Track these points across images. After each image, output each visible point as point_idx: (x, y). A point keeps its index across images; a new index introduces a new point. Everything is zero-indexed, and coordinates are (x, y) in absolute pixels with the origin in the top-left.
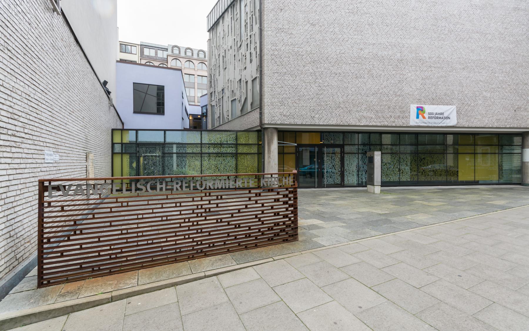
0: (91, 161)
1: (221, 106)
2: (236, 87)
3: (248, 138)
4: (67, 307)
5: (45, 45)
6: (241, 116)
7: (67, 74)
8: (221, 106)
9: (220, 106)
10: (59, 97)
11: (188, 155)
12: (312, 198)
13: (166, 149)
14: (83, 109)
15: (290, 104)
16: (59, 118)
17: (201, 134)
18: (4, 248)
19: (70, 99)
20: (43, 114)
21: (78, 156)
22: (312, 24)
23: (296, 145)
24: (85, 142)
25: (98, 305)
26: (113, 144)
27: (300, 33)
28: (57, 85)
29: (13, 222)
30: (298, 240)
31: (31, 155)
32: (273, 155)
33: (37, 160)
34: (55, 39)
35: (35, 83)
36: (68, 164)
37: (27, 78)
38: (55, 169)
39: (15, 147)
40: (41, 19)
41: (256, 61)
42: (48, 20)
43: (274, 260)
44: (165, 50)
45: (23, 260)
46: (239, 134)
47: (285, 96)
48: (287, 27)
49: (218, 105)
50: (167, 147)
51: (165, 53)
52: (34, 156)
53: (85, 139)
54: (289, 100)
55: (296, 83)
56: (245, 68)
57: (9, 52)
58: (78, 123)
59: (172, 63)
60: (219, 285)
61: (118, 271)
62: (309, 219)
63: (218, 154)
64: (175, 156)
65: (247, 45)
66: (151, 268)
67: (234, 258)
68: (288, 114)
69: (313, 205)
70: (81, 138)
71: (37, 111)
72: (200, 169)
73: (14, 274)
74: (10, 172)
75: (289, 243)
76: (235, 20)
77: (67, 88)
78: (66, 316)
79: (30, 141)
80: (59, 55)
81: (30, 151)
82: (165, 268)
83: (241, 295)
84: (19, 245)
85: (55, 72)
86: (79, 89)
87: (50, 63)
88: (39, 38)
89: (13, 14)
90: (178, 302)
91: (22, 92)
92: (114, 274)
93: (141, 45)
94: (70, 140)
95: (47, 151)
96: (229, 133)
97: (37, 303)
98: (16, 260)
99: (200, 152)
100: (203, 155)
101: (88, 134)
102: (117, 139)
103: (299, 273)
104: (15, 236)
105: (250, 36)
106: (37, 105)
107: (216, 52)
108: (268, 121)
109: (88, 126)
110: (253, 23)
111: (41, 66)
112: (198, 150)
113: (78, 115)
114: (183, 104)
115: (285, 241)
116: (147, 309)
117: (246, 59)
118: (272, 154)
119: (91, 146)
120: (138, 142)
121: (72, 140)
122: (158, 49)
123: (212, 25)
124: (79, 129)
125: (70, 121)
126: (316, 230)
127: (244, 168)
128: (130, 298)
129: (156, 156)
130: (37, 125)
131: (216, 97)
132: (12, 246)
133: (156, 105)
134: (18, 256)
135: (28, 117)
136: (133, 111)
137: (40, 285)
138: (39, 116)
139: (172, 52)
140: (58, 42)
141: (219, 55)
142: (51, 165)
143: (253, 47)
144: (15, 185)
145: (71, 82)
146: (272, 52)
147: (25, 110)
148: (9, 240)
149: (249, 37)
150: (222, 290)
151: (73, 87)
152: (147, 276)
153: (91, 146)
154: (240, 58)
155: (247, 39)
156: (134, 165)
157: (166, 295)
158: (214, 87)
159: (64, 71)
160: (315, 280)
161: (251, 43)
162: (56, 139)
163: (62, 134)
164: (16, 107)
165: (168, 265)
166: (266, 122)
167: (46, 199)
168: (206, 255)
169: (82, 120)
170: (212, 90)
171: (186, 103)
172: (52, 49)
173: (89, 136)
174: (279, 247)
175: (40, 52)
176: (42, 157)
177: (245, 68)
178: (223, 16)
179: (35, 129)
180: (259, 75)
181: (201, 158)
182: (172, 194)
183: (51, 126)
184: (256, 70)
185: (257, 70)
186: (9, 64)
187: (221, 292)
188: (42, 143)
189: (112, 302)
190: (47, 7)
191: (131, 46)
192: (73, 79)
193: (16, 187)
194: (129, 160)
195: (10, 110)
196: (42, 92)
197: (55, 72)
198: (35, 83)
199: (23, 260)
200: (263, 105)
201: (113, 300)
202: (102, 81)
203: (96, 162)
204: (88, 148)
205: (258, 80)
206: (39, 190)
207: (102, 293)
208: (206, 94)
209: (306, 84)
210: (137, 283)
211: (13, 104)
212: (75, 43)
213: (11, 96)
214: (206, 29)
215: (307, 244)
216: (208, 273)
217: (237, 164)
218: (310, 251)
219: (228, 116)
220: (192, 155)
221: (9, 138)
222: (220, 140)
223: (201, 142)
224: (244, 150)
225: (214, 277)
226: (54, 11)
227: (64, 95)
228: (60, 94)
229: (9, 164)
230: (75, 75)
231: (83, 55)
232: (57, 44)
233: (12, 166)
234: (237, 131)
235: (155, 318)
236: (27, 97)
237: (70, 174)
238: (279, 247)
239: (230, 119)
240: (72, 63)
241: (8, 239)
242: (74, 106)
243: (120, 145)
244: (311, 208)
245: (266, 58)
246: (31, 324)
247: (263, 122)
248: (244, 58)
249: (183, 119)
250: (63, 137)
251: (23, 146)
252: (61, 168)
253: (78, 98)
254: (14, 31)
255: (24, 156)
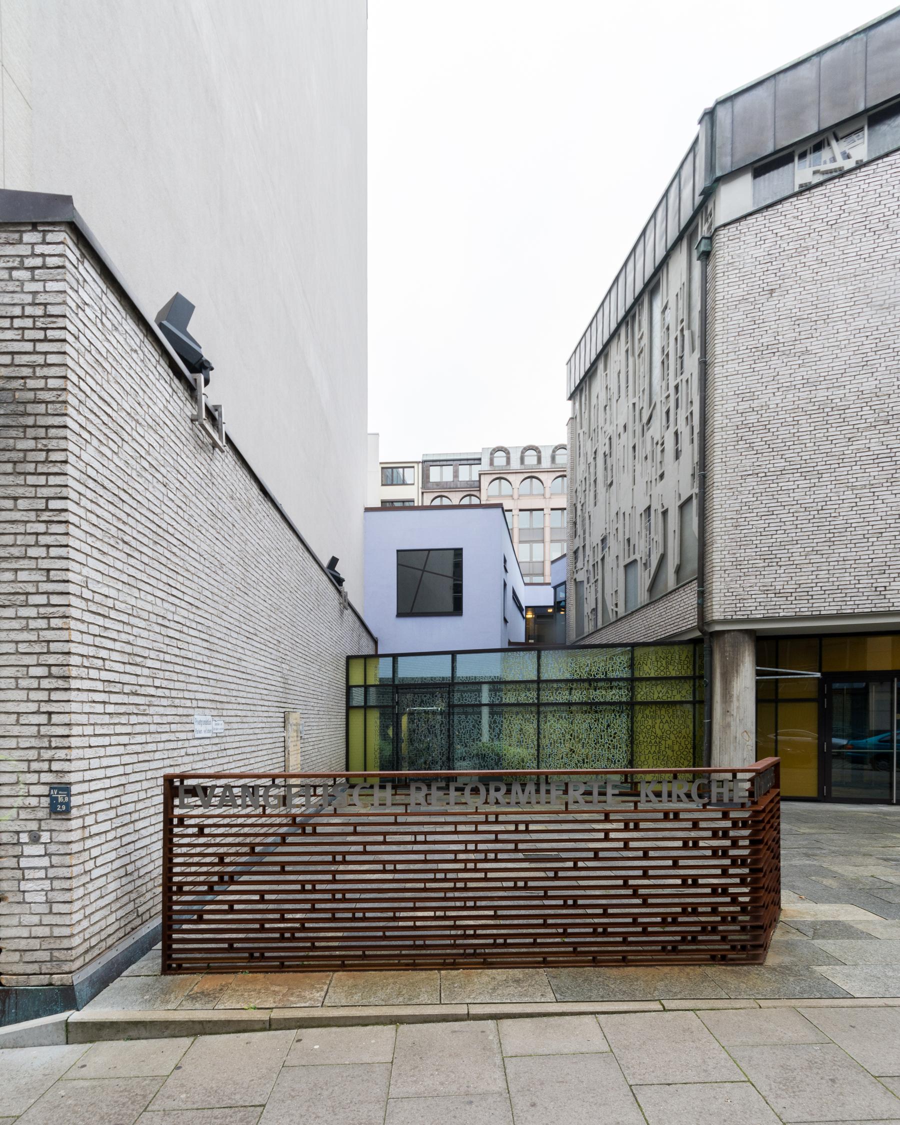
0: (295, 728)
1: (600, 582)
2: (638, 529)
3: (664, 662)
4: (193, 1022)
5: (196, 517)
6: (647, 605)
7: (241, 562)
8: (600, 582)
9: (596, 581)
10: (225, 610)
11: (505, 709)
12: (867, 836)
13: (457, 696)
14: (278, 624)
15: (797, 559)
16: (225, 651)
17: (539, 658)
18: (115, 893)
19: (248, 610)
20: (192, 648)
21: (265, 720)
22: (882, 307)
23: (818, 675)
24: (281, 690)
25: (245, 1031)
26: (349, 688)
27: (838, 343)
28: (221, 587)
29: (131, 847)
30: (761, 964)
31: (168, 726)
32: (738, 708)
33: (177, 735)
34: (218, 500)
35: (175, 592)
36: (243, 738)
37: (161, 585)
38: (215, 748)
39: (137, 714)
40: (188, 469)
41: (690, 452)
42: (202, 468)
43: (665, 1010)
44: (476, 462)
45: (151, 917)
46: (639, 652)
47: (780, 537)
48: (791, 335)
49: (592, 581)
50: (458, 691)
51: (476, 469)
52: (174, 727)
53: (282, 685)
54: (795, 549)
55: (821, 493)
56: (662, 476)
57: (126, 546)
58: (266, 654)
59: (489, 492)
60: (495, 1046)
61: (298, 966)
62: (828, 901)
63: (592, 706)
64: (485, 711)
65: (668, 412)
66: (358, 973)
67: (554, 982)
68: (790, 588)
69: (860, 860)
70: (274, 683)
71: (180, 644)
72: (536, 743)
73: (133, 942)
74: (126, 759)
75: (729, 968)
76: (637, 353)
77: (243, 588)
78: (192, 1039)
79: (166, 700)
80: (225, 528)
81: (165, 720)
82: (387, 979)
83: (542, 1084)
84: (144, 889)
85: (216, 563)
86: (269, 586)
87: (207, 548)
88: (183, 506)
89: (134, 475)
90: (392, 1062)
91: (149, 612)
92: (288, 972)
93: (424, 462)
94: (248, 689)
95: (198, 716)
96: (612, 651)
97: (152, 1002)
98: (138, 916)
99: (536, 701)
100: (542, 709)
101: (289, 673)
102: (357, 678)
103: (731, 1062)
104: (136, 875)
105: (677, 387)
106: (180, 632)
107: (588, 447)
108: (724, 612)
109: (288, 658)
110: (683, 351)
111: (187, 558)
112: (529, 696)
113: (266, 638)
114: (505, 585)
115: (718, 959)
116: (327, 1062)
117: (663, 451)
118: (735, 704)
119: (296, 697)
120: (396, 683)
121: (253, 690)
122: (459, 462)
123: (578, 382)
124: (268, 666)
125: (247, 652)
126: (839, 942)
127: (653, 741)
128: (304, 1030)
129: (434, 713)
130: (178, 669)
131: (586, 559)
132: (131, 892)
133: (452, 591)
134: (141, 910)
135: (161, 656)
136: (395, 613)
137: (167, 969)
138: (183, 653)
139: (492, 463)
140: (223, 504)
141: (595, 453)
142: (207, 742)
143: (684, 417)
144: (137, 782)
145: (250, 576)
146: (737, 420)
147: (155, 644)
148: (124, 881)
149: (672, 391)
150: (498, 1061)
151: (255, 585)
152: (346, 988)
153: (296, 697)
154: (648, 452)
155: (668, 397)
156: (390, 732)
157: (373, 1041)
158: (582, 536)
159: (236, 558)
160: (778, 1096)
161: (677, 407)
162: (218, 691)
163: (231, 679)
164: (139, 642)
165: (395, 972)
166: (717, 615)
167: (177, 811)
168: (487, 964)
169: (276, 647)
170: (578, 543)
171: (516, 580)
172: (210, 521)
173: (291, 678)
174: (691, 973)
175: (186, 533)
176: (188, 727)
177: (662, 476)
178: (605, 352)
179: (175, 677)
180: (696, 490)
181: (539, 717)
182: (406, 814)
183: (207, 667)
184: (689, 478)
185: (693, 475)
186: (126, 568)
187: (495, 1065)
188: (189, 701)
189: (270, 1030)
190: (200, 442)
191: (404, 468)
192: (257, 569)
193: (138, 786)
194: (378, 721)
195: (128, 649)
196: (189, 607)
197: (216, 563)
198: (175, 592)
199: (151, 917)
200: (707, 570)
201: (273, 1027)
202: (325, 563)
203: (307, 728)
204: (290, 701)
205: (693, 509)
206: (164, 794)
207: (255, 1008)
208: (564, 556)
209: (855, 492)
210: (321, 999)
211: (134, 638)
212: (261, 497)
213: (128, 624)
214: (565, 394)
215: (791, 979)
216: (475, 1010)
217: (632, 730)
218: (793, 1002)
219: (616, 605)
220: (515, 709)
221: (125, 699)
222: (588, 669)
223: (539, 677)
224: (658, 693)
225: (491, 1023)
226: (214, 448)
227: (236, 604)
228: (227, 604)
229: (125, 745)
230: (259, 560)
231: (277, 516)
232: (220, 509)
233: (130, 749)
234: (634, 645)
235: (336, 1088)
236: (160, 621)
237: (248, 756)
238: (691, 973)
239: (620, 615)
240: (255, 538)
241: (123, 879)
242: (257, 622)
243: (363, 689)
244: (851, 868)
245: (718, 438)
246: (139, 1039)
247: (709, 618)
248: (659, 448)
249: (506, 621)
250: (233, 686)
251: (152, 710)
252: (227, 746)
253: (266, 605)
254: (135, 506)
255: (153, 728)
